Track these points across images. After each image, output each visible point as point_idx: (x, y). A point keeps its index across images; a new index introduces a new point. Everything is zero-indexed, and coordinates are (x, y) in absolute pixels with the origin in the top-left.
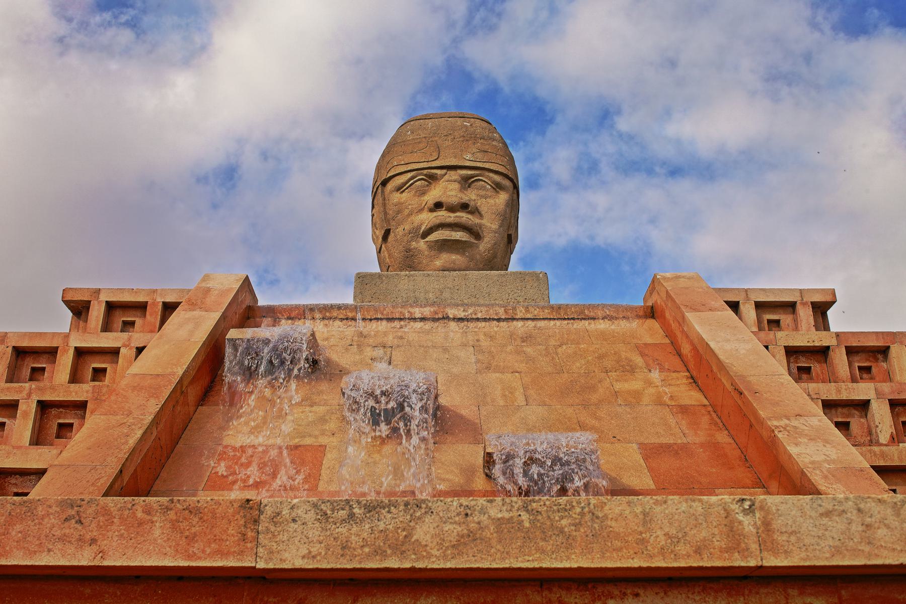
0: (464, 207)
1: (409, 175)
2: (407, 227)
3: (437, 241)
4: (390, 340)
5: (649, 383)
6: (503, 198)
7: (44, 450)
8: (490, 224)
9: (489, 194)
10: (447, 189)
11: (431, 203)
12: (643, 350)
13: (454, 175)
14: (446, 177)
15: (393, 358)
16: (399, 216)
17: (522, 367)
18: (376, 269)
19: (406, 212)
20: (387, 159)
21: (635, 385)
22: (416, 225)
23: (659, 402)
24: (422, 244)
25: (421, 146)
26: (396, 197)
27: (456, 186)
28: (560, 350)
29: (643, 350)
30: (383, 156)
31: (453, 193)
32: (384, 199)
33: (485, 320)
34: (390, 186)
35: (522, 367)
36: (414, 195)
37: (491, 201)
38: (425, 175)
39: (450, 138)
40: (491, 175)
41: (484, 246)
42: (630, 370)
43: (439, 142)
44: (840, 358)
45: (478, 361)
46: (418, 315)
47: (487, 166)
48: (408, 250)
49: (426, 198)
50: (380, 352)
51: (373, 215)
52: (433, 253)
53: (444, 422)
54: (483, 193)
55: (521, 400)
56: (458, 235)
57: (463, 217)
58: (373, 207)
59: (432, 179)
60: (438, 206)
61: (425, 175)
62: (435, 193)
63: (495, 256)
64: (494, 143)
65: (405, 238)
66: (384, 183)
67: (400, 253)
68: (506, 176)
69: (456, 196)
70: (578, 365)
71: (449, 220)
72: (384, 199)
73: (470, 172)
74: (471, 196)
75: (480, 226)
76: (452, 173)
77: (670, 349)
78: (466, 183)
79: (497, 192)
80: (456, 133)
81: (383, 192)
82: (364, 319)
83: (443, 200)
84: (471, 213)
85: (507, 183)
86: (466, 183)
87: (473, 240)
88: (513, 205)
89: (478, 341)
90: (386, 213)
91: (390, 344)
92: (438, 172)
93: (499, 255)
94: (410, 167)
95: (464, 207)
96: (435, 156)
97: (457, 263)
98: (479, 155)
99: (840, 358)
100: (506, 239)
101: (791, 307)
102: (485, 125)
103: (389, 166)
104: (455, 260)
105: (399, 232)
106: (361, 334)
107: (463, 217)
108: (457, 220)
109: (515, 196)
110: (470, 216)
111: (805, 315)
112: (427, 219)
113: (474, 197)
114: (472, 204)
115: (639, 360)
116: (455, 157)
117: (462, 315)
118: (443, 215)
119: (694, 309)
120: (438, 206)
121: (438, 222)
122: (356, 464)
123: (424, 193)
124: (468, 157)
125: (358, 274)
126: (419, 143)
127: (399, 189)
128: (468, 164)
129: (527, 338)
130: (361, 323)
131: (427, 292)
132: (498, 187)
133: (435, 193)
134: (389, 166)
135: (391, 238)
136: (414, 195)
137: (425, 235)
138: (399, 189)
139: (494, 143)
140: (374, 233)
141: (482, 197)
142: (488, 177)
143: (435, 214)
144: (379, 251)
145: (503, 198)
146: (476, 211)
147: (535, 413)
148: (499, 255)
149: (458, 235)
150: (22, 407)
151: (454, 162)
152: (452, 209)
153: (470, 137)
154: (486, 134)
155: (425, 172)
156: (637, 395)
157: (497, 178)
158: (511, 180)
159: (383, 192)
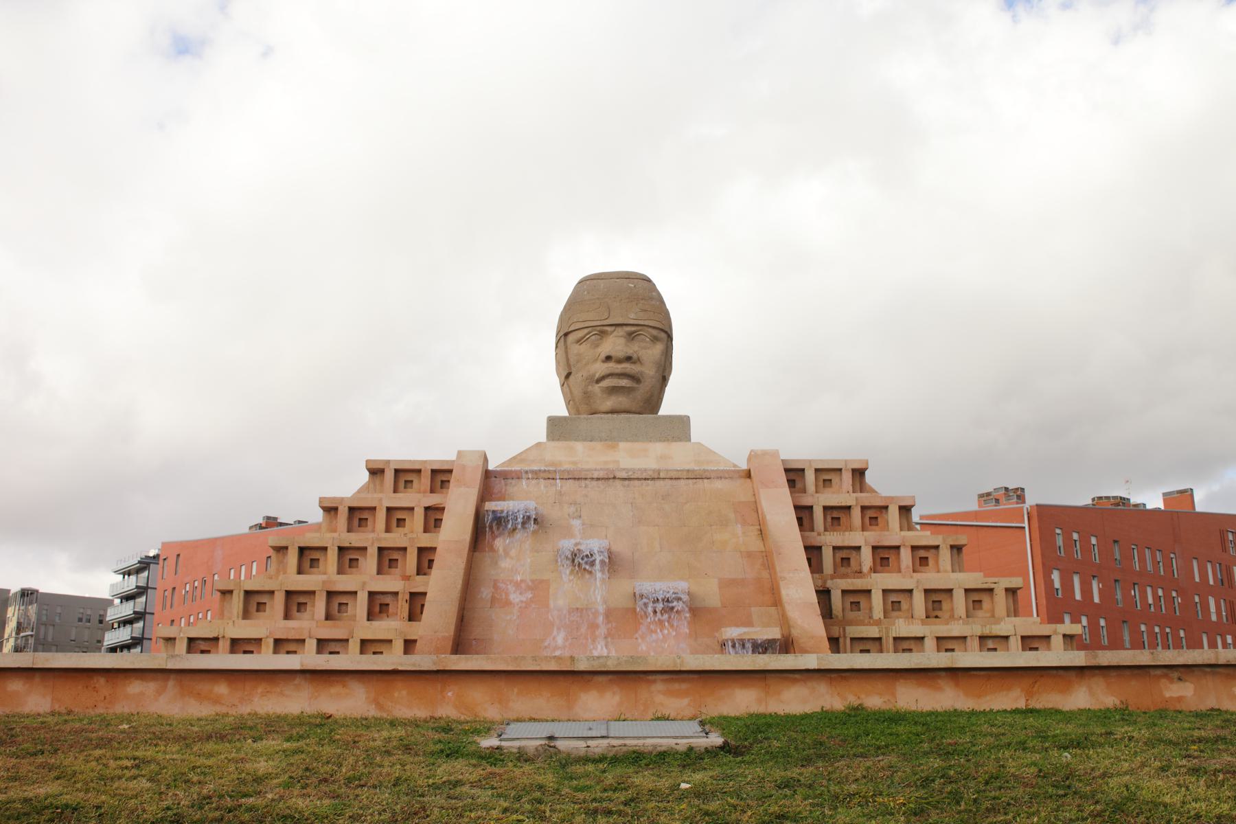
0: (629, 359)
1: (586, 331)
6: (659, 348)
7: (376, 623)
8: (649, 371)
10: (615, 344)
11: (603, 356)
13: (621, 331)
18: (566, 413)
24: (596, 388)
26: (575, 349)
27: (622, 341)
34: (571, 338)
37: (650, 352)
41: (643, 389)
47: (646, 323)
49: (599, 350)
50: (572, 509)
54: (643, 344)
56: (624, 382)
59: (602, 334)
60: (608, 358)
63: (652, 396)
66: (566, 335)
68: (662, 330)
73: (633, 329)
74: (633, 349)
75: (642, 373)
78: (631, 336)
81: (565, 341)
83: (613, 354)
85: (663, 335)
86: (631, 336)
87: (635, 385)
90: (568, 360)
92: (609, 329)
94: (587, 324)
95: (629, 359)
106: (560, 494)
110: (633, 366)
112: (601, 368)
113: (636, 348)
114: (635, 356)
115: (732, 516)
120: (608, 358)
121: (608, 372)
122: (566, 590)
123: (597, 346)
124: (632, 316)
127: (579, 341)
128: (632, 322)
132: (655, 339)
135: (572, 377)
137: (598, 381)
138: (579, 341)
143: (606, 365)
145: (659, 348)
149: (624, 382)
150: (369, 550)
151: (620, 321)
152: (619, 361)
157: (655, 332)
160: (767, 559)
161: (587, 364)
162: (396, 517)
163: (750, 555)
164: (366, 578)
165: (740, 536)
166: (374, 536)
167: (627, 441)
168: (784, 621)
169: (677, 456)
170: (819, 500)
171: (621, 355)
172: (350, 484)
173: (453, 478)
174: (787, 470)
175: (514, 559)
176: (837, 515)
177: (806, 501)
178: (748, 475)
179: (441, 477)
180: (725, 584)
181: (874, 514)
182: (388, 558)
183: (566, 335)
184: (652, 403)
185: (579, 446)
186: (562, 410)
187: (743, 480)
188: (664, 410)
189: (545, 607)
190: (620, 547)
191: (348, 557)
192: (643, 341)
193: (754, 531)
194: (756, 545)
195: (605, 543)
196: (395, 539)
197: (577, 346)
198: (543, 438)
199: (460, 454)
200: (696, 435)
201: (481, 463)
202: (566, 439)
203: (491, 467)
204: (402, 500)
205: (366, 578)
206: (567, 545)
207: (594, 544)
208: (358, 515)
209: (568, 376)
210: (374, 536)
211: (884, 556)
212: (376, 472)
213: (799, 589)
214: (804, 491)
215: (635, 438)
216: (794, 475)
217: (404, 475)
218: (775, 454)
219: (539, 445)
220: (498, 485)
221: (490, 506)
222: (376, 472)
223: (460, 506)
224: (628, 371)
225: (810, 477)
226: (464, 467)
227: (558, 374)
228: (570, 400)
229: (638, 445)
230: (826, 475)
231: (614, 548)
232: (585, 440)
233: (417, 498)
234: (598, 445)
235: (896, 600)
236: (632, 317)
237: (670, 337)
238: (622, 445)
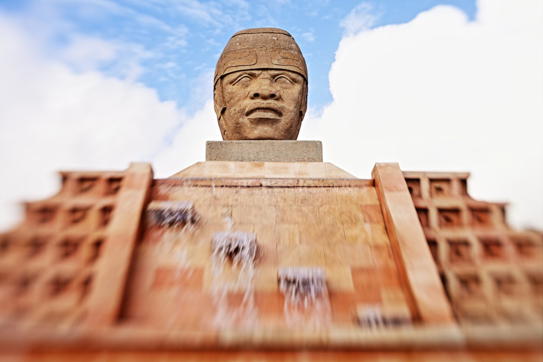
0: (272, 96)
2: (237, 109)
3: (255, 119)
4: (230, 202)
5: (363, 231)
6: (297, 88)
8: (288, 106)
9: (288, 86)
10: (262, 85)
11: (252, 94)
12: (364, 209)
13: (266, 74)
14: (261, 76)
15: (233, 214)
16: (232, 101)
17: (300, 220)
18: (221, 139)
19: (236, 99)
20: (224, 62)
21: (354, 231)
22: (242, 107)
23: (366, 242)
24: (245, 120)
25: (246, 54)
26: (230, 88)
27: (268, 82)
28: (321, 209)
29: (364, 209)
30: (222, 58)
31: (265, 87)
32: (222, 88)
33: (282, 187)
34: (226, 80)
35: (300, 220)
36: (241, 88)
38: (248, 74)
39: (264, 49)
40: (290, 73)
41: (284, 121)
42: (354, 221)
43: (257, 51)
44: (466, 216)
45: (277, 216)
46: (245, 185)
48: (237, 123)
49: (248, 89)
50: (225, 210)
51: (215, 94)
52: (253, 126)
53: (258, 255)
55: (297, 241)
56: (269, 115)
57: (272, 103)
58: (215, 89)
59: (252, 76)
60: (256, 95)
61: (248, 74)
62: (255, 87)
63: (291, 126)
64: (292, 52)
65: (236, 116)
66: (222, 77)
67: (232, 124)
69: (267, 89)
70: (328, 220)
71: (263, 106)
72: (222, 88)
74: (276, 88)
75: (283, 108)
76: (265, 72)
77: (379, 209)
79: (293, 84)
80: (268, 46)
81: (221, 83)
82: (216, 186)
83: (259, 92)
84: (277, 100)
85: (300, 78)
87: (278, 118)
88: (304, 93)
89: (277, 202)
90: (223, 98)
91: (230, 204)
93: (294, 125)
95: (272, 96)
96: (254, 61)
97: (268, 131)
98: (283, 61)
99: (466, 216)
100: (298, 114)
101: (447, 181)
102: (287, 38)
103: (225, 67)
104: (266, 130)
105: (231, 111)
106: (216, 198)
107: (272, 103)
108: (268, 106)
109: (305, 85)
110: (276, 102)
111: (456, 186)
112: (249, 104)
113: (279, 89)
114: (277, 94)
115: (361, 216)
116: (267, 63)
117: (269, 184)
118: (259, 102)
119: (390, 190)
120: (256, 95)
121: (256, 106)
122: (219, 279)
124: (276, 62)
125: (207, 142)
126: (245, 52)
128: (275, 67)
129: (304, 201)
130: (214, 189)
131: (249, 154)
132: (294, 81)
133: (255, 87)
134: (225, 67)
135: (227, 112)
136: (241, 88)
137: (248, 114)
139: (292, 52)
140: (215, 106)
141: (284, 88)
142: (289, 76)
143: (254, 101)
144: (219, 119)
146: (279, 99)
147: (304, 249)
148: (294, 125)
149: (269, 115)
152: (265, 98)
153: (277, 48)
154: (287, 45)
155: (248, 72)
156: (355, 239)
157: (294, 76)
158: (302, 76)
159: (221, 83)
160: (395, 250)
161: (239, 100)
162: (77, 214)
163: (377, 248)
164: (48, 264)
165: (374, 232)
166: (57, 229)
167: (271, 160)
168: (412, 301)
169: (312, 171)
170: (434, 203)
171: (266, 93)
172: (44, 188)
173: (124, 183)
174: (408, 180)
175: (170, 251)
176: (449, 215)
177: (422, 204)
178: (374, 183)
179: (114, 183)
180: (355, 272)
181: (480, 213)
182: (69, 247)
183: (222, 77)
184: (292, 132)
185: (232, 165)
186: (218, 137)
187: (368, 188)
188: (301, 137)
189: (200, 289)
190: (265, 241)
191: (36, 245)
192: (284, 82)
193: (380, 227)
194: (382, 239)
195: (252, 237)
196: (76, 231)
197: (230, 86)
198: (202, 158)
199: (132, 165)
200: (326, 158)
201: (147, 171)
202: (221, 159)
203: (157, 176)
204: (83, 200)
205: (48, 264)
206: (222, 239)
207: (245, 239)
208: (44, 212)
209: (223, 111)
210: (57, 229)
211: (491, 247)
212: (65, 177)
213: (423, 275)
214: (420, 196)
215: (277, 159)
216: (413, 182)
217: (86, 182)
218: (396, 166)
219: (198, 164)
220: (162, 190)
221: (153, 205)
222: (65, 177)
223: (128, 207)
224: (272, 106)
225: (425, 185)
226: (133, 175)
227: (216, 111)
228: (223, 133)
229: (280, 165)
230: (439, 183)
231: (260, 242)
232: (237, 160)
233: (94, 200)
234: (247, 164)
235: (503, 283)
236: (275, 63)
237: (306, 80)
238: (267, 164)
